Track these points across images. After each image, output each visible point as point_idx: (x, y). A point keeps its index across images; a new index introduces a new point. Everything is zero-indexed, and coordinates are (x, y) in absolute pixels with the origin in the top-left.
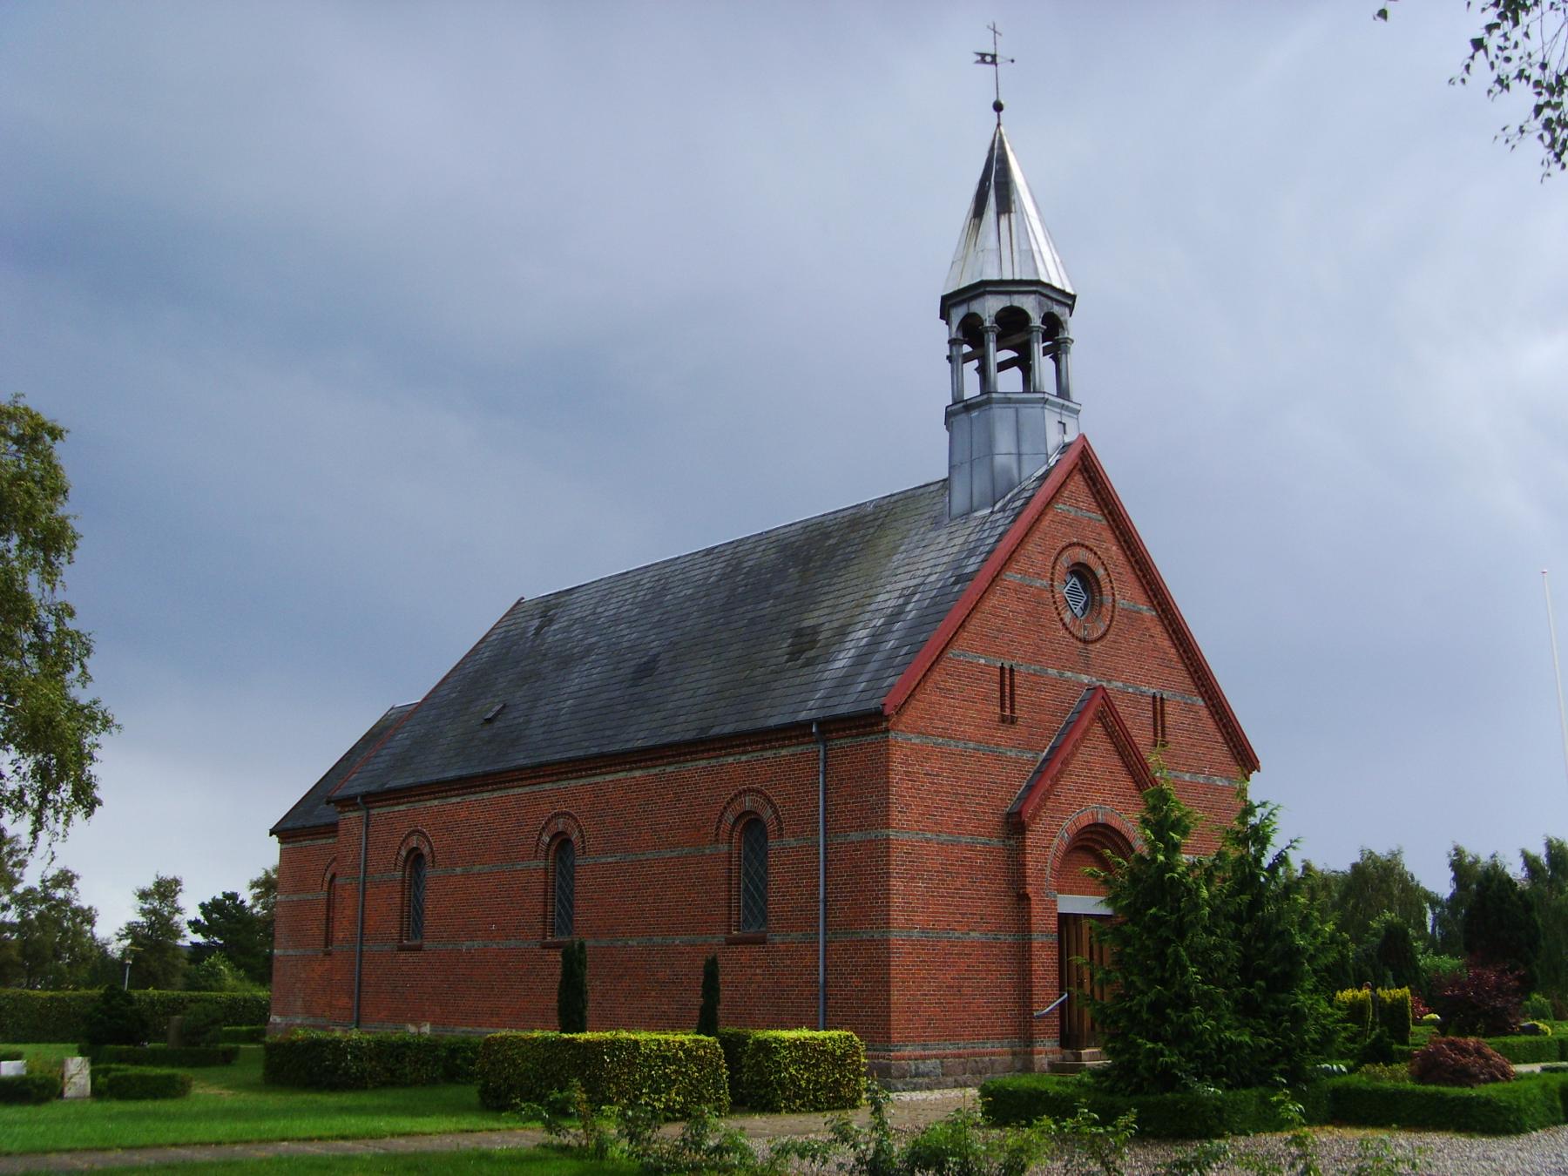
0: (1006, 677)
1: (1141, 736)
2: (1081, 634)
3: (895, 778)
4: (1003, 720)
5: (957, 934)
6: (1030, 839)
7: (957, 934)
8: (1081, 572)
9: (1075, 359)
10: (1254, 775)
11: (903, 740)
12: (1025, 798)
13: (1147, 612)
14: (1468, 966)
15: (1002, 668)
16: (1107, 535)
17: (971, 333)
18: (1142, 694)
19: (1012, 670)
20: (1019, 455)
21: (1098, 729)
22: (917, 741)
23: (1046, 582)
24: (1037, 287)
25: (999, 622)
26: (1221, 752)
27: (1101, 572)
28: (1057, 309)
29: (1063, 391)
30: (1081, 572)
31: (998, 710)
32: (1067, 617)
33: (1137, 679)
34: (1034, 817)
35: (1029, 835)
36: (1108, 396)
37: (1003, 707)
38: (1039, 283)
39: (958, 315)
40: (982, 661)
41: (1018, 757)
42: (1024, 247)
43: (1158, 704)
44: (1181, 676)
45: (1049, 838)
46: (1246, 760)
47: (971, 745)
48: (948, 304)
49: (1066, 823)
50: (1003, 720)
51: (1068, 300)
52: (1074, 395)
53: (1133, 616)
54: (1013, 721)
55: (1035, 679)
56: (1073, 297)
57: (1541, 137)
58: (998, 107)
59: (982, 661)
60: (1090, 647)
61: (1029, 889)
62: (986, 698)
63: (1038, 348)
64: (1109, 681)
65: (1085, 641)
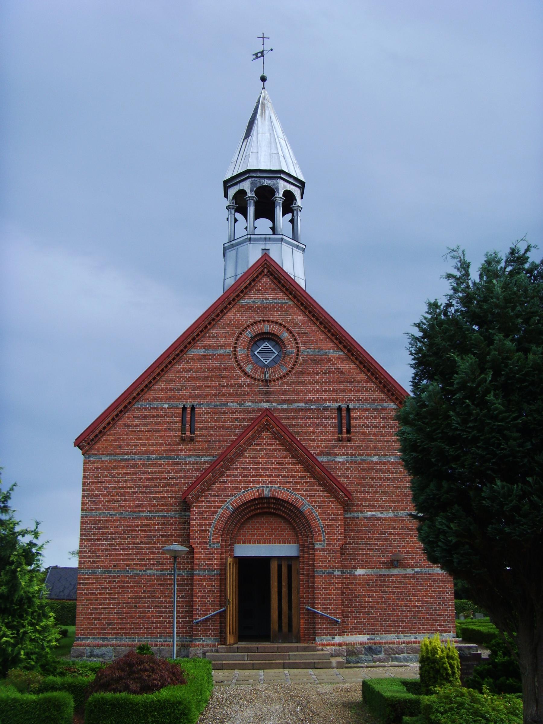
2: (263, 377)
5: (134, 571)
7: (134, 571)
9: (301, 218)
13: (332, 352)
14: (474, 284)
15: (184, 408)
17: (239, 205)
18: (325, 408)
19: (193, 408)
22: (107, 459)
25: (182, 380)
29: (295, 236)
32: (249, 369)
34: (198, 497)
37: (184, 431)
39: (232, 192)
40: (166, 406)
41: (194, 460)
43: (344, 416)
47: (154, 457)
48: (227, 184)
50: (183, 439)
51: (301, 185)
52: (301, 239)
53: (317, 360)
54: (192, 440)
55: (214, 411)
56: (303, 183)
59: (166, 406)
63: (279, 211)
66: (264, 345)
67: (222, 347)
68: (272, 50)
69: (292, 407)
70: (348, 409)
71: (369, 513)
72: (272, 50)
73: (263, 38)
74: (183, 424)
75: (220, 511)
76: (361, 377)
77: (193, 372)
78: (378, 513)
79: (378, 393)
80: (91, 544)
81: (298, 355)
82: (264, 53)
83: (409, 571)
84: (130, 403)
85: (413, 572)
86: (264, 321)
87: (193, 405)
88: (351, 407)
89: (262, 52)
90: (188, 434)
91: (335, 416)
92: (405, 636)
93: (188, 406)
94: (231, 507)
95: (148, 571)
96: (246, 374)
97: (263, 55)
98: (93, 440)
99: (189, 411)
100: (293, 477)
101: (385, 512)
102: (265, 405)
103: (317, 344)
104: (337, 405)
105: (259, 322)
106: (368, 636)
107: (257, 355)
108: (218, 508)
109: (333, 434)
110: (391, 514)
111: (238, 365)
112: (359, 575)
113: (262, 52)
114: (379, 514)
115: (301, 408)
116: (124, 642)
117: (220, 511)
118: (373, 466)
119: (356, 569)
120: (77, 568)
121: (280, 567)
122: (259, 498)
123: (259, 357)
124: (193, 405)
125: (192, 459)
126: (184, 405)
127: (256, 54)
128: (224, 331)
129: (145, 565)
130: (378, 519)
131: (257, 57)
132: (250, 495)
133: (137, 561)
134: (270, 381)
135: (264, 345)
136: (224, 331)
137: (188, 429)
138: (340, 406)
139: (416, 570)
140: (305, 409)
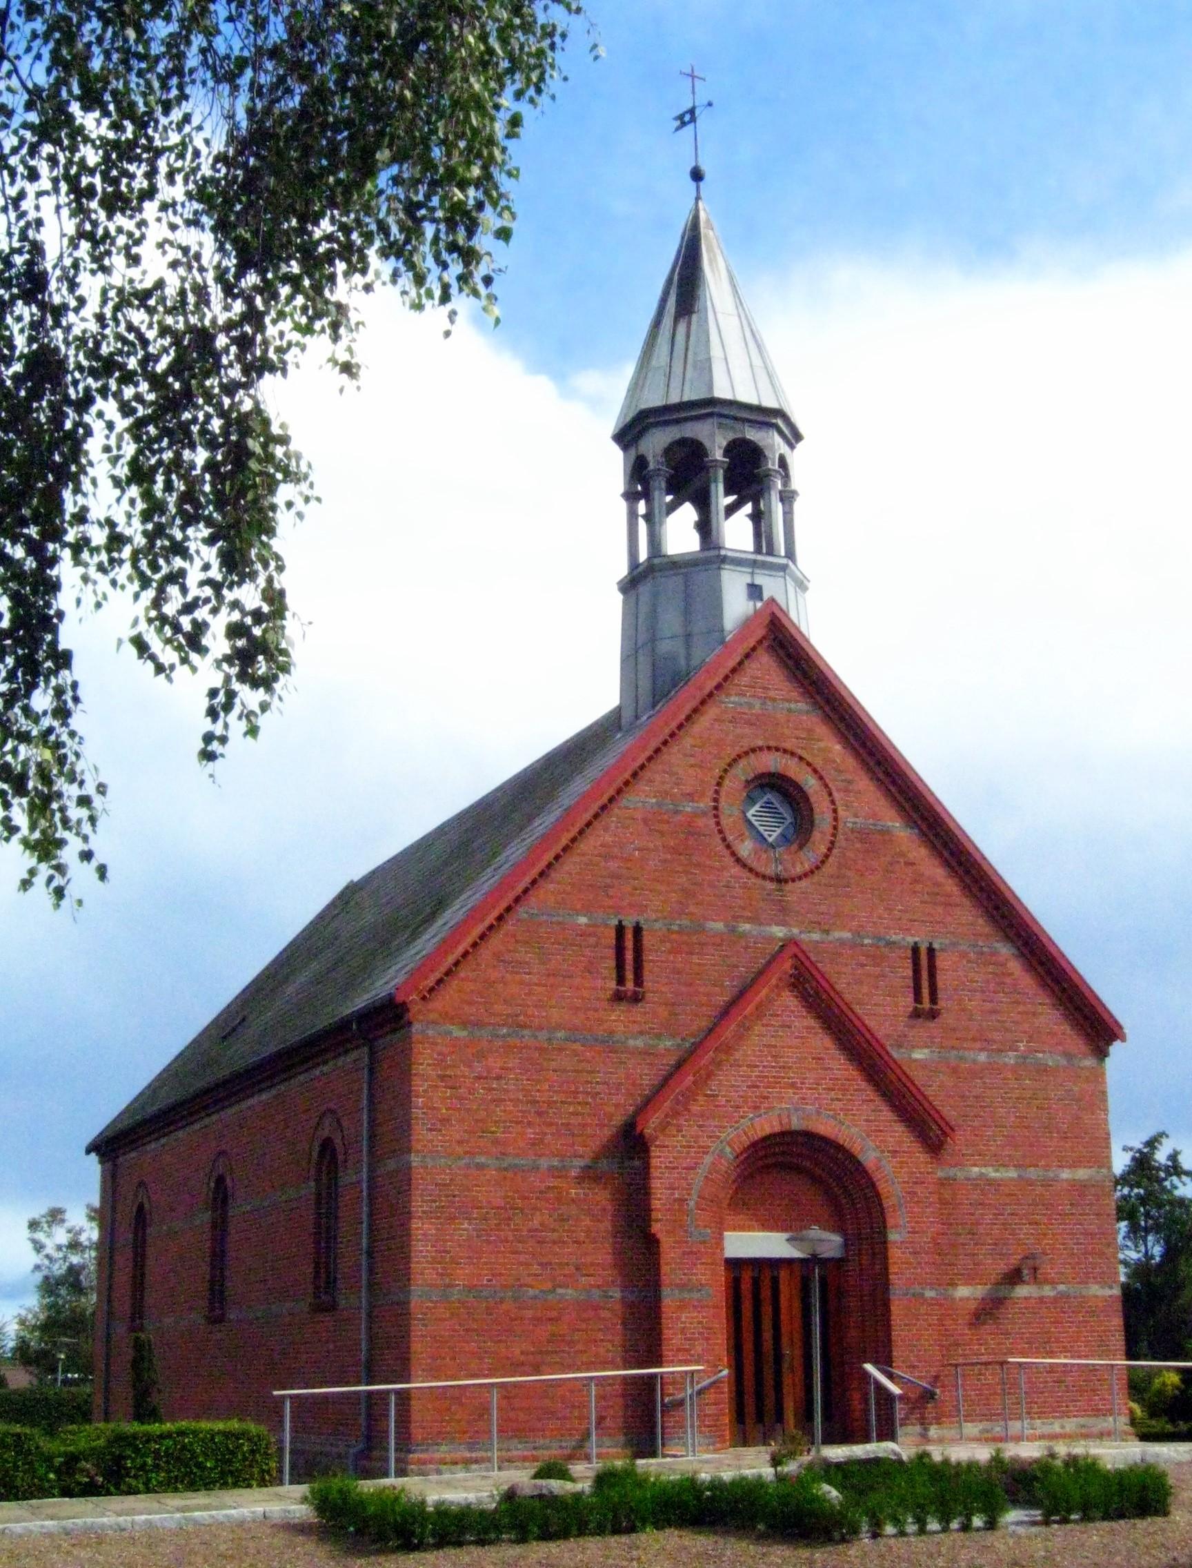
0: (628, 950)
1: (881, 1007)
2: (771, 870)
3: (419, 1086)
4: (618, 997)
5: (531, 1292)
6: (659, 1159)
8: (777, 786)
9: (798, 506)
10: (1116, 1048)
11: (432, 1043)
12: (646, 1104)
13: (895, 824)
16: (822, 730)
18: (890, 944)
19: (638, 930)
20: (688, 636)
21: (789, 1000)
23: (705, 804)
24: (710, 408)
25: (613, 865)
26: (1049, 1017)
27: (810, 783)
28: (752, 435)
30: (777, 786)
31: (612, 985)
32: (746, 848)
33: (863, 924)
34: (663, 1127)
35: (655, 1152)
36: (220, 759)
37: (621, 980)
38: (712, 402)
39: (655, 443)
40: (583, 920)
42: (702, 357)
43: (924, 964)
44: (967, 917)
45: (692, 1157)
46: (1097, 1028)
47: (560, 1034)
49: (729, 1133)
50: (618, 997)
57: (310, 466)
58: (697, 175)
60: (789, 886)
61: (656, 1228)
62: (590, 969)
64: (827, 932)
65: (779, 880)
66: (765, 799)
67: (690, 796)
68: (710, 104)
69: (830, 938)
70: (931, 951)
71: (976, 1169)
72: (710, 104)
73: (693, 77)
74: (620, 966)
75: (708, 1159)
76: (951, 887)
77: (635, 849)
78: (990, 1169)
79: (982, 925)
80: (437, 1229)
81: (835, 828)
82: (697, 112)
83: (1048, 1291)
84: (509, 909)
85: (1052, 1294)
86: (769, 748)
87: (638, 923)
88: (936, 946)
89: (692, 111)
90: (630, 985)
91: (909, 964)
92: (1043, 1423)
93: (629, 923)
94: (728, 1150)
95: (560, 1291)
96: (738, 860)
97: (693, 120)
98: (431, 990)
99: (629, 936)
100: (845, 1090)
101: (1001, 1169)
102: (779, 932)
103: (864, 804)
104: (911, 940)
105: (761, 749)
106: (981, 1426)
107: (753, 819)
108: (704, 1153)
109: (906, 1002)
110: (1012, 1173)
111: (724, 839)
112: (961, 1299)
113: (692, 111)
114: (992, 1173)
115: (842, 943)
116: (515, 1453)
117: (708, 1159)
118: (976, 1072)
119: (953, 1284)
120: (840, 1260)
121: (756, 1282)
122: (783, 1134)
123: (756, 824)
124: (638, 923)
125: (639, 1043)
126: (620, 922)
127: (680, 118)
128: (692, 760)
129: (553, 1279)
130: (991, 1182)
131: (683, 124)
132: (766, 1125)
133: (536, 1269)
134: (786, 881)
135: (765, 799)
136: (692, 760)
137: (629, 975)
138: (916, 943)
139: (1062, 1287)
140: (853, 946)
